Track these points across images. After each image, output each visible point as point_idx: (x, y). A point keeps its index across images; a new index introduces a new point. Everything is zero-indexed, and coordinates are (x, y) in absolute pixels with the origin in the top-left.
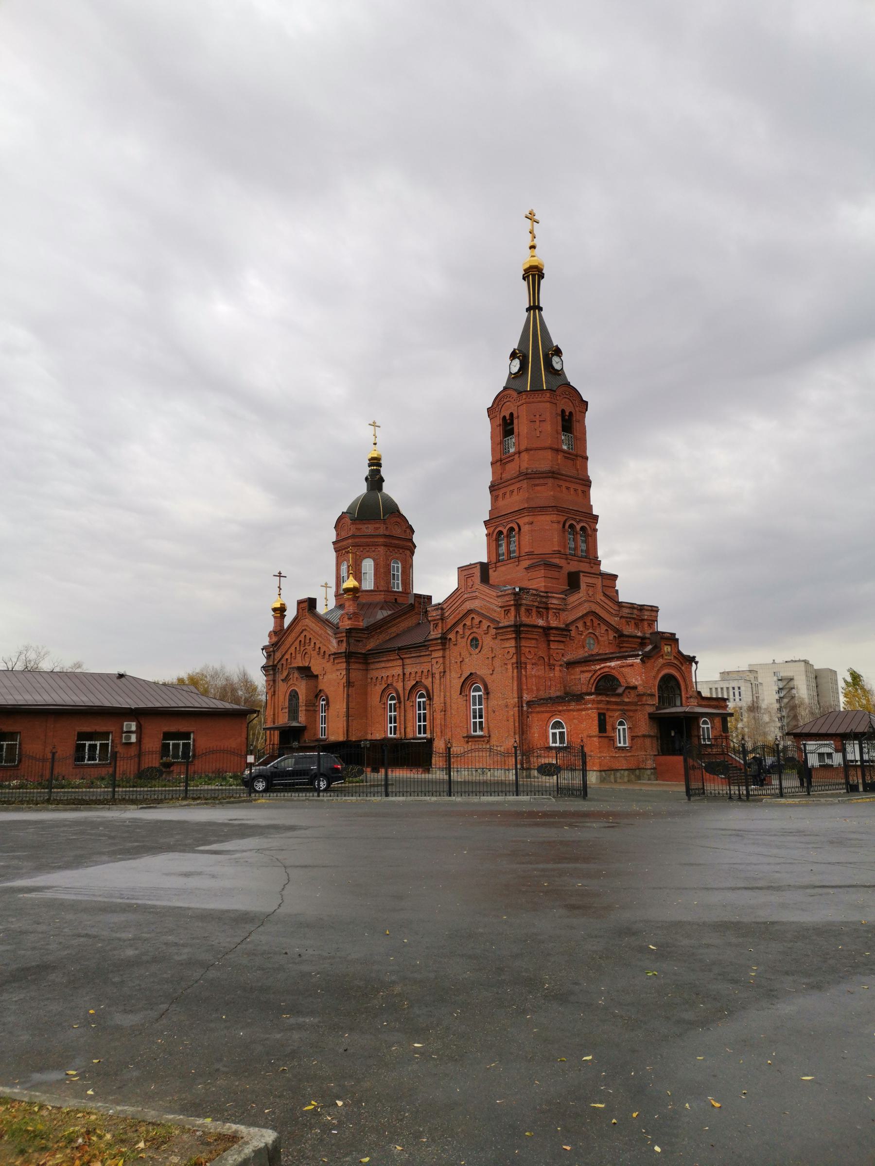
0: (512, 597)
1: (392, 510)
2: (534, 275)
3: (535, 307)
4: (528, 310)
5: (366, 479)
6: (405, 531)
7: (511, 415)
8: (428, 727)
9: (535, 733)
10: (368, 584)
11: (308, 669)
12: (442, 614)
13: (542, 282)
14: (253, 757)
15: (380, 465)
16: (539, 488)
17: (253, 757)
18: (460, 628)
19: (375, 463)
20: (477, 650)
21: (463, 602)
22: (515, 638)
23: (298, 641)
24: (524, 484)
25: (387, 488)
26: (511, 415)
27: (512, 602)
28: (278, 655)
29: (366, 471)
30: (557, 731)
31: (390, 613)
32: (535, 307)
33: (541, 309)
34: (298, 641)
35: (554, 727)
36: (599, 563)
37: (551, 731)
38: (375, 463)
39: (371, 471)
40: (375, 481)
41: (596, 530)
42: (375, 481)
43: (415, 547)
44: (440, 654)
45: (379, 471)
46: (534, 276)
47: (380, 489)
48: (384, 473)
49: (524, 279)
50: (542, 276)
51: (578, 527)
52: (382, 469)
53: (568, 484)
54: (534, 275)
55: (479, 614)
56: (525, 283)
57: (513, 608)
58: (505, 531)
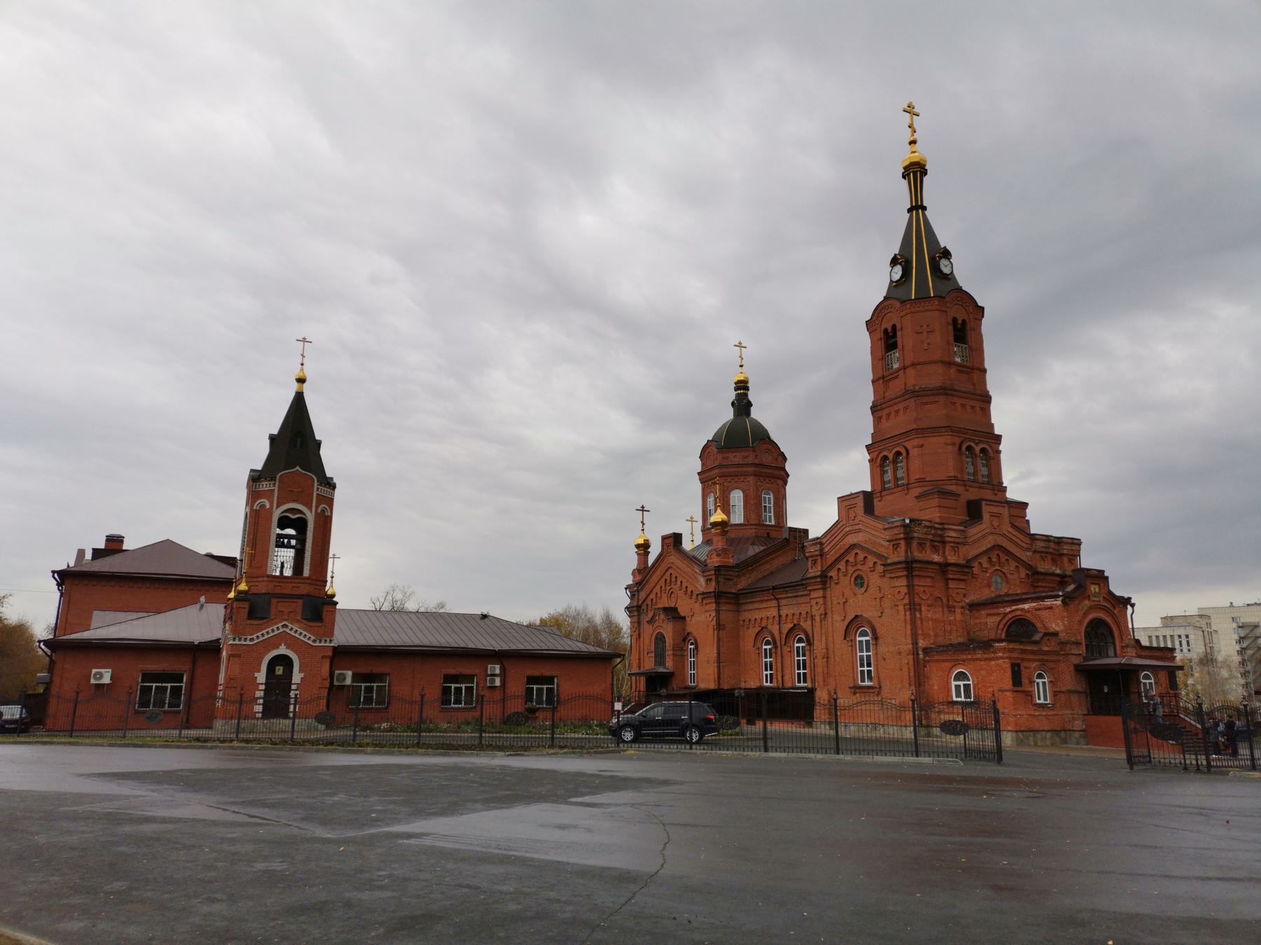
1: (762, 436)
2: (915, 172)
3: (917, 207)
4: (910, 211)
5: (733, 404)
7: (894, 327)
9: (934, 685)
10: (738, 518)
11: (675, 610)
12: (821, 550)
13: (925, 179)
15: (747, 389)
18: (842, 565)
19: (742, 386)
20: (863, 590)
22: (907, 577)
24: (911, 403)
25: (755, 413)
26: (894, 327)
28: (643, 595)
29: (732, 395)
30: (961, 683)
32: (917, 207)
33: (924, 208)
37: (954, 683)
38: (742, 386)
40: (742, 405)
41: (999, 452)
42: (742, 405)
45: (746, 395)
46: (915, 173)
47: (748, 414)
48: (751, 396)
49: (904, 177)
50: (924, 172)
51: (977, 449)
53: (896, 408)
54: (915, 172)
55: (863, 549)
56: (905, 182)
57: (902, 542)
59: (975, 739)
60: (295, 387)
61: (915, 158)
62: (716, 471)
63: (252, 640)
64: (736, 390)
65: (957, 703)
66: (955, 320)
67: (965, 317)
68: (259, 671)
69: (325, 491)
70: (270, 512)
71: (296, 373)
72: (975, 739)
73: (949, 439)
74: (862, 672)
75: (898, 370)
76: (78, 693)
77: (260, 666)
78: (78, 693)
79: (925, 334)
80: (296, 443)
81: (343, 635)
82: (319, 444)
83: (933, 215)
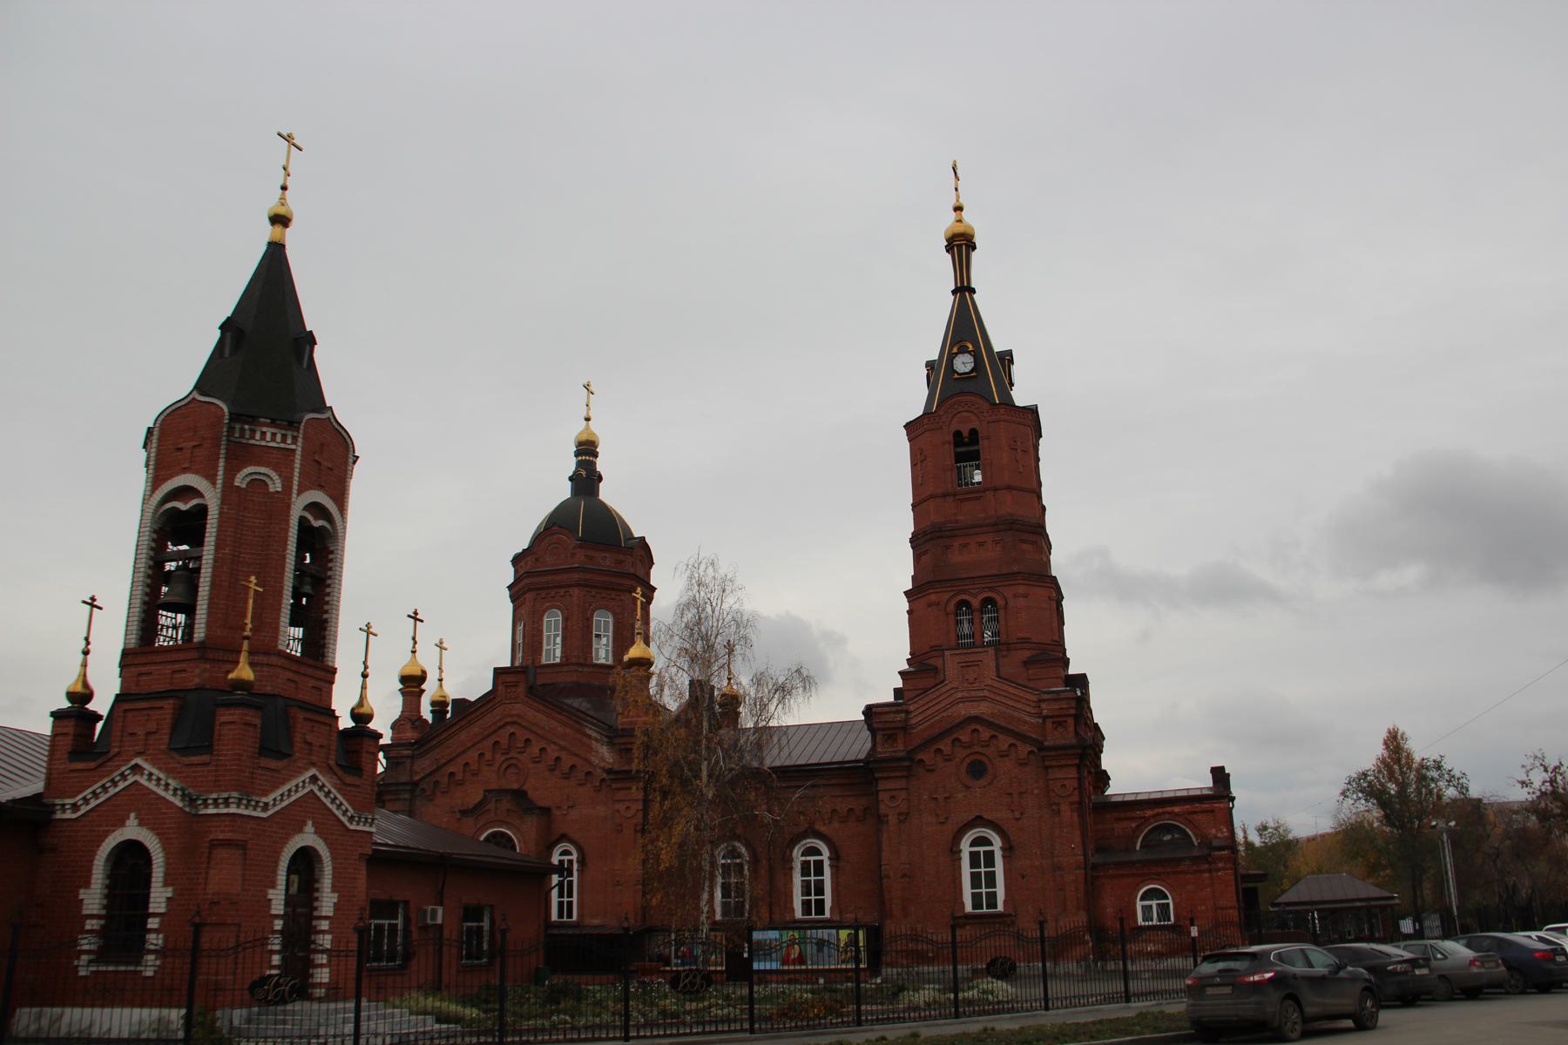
0: (1073, 704)
2: (961, 245)
3: (963, 290)
4: (954, 292)
9: (1109, 907)
11: (520, 795)
12: (906, 720)
14: (1402, 923)
16: (1025, 547)
17: (1402, 923)
18: (945, 745)
19: (587, 450)
20: (983, 782)
21: (952, 704)
22: (1078, 767)
23: (491, 741)
26: (973, 432)
27: (1073, 712)
28: (424, 765)
29: (570, 465)
30: (1154, 903)
31: (569, 701)
32: (963, 290)
33: (973, 291)
34: (491, 741)
35: (972, 845)
36: (1066, 662)
37: (1139, 905)
38: (587, 450)
39: (579, 464)
40: (586, 479)
42: (586, 479)
44: (902, 783)
46: (959, 246)
47: (594, 491)
48: (601, 465)
51: (976, 603)
54: (961, 245)
55: (990, 725)
56: (949, 257)
57: (1071, 721)
58: (976, 603)
60: (265, 233)
61: (960, 229)
62: (576, 576)
63: (75, 807)
64: (577, 454)
66: (958, 434)
67: (975, 425)
68: (87, 885)
70: (282, 503)
71: (271, 203)
74: (570, 895)
77: (275, 872)
80: (264, 356)
82: (913, 429)
83: (983, 300)
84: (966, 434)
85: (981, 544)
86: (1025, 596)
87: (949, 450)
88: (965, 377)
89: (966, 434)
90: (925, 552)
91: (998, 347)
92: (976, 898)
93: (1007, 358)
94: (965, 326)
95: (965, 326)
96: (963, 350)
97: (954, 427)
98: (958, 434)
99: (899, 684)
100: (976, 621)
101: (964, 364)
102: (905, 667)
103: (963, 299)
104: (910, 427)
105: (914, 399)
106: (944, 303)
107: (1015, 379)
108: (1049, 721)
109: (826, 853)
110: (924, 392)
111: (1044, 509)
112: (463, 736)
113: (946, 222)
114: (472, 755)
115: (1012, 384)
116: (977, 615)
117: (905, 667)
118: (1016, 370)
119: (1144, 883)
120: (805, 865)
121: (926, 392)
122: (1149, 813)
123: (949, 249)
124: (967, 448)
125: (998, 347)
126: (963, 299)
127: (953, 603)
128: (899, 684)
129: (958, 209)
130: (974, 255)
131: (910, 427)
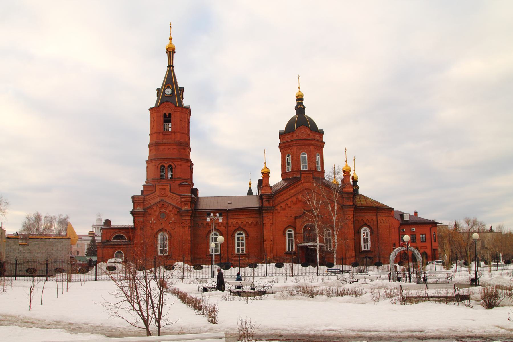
2: (171, 52)
3: (171, 66)
6: (309, 135)
7: (170, 114)
8: (293, 234)
15: (302, 100)
19: (300, 99)
22: (191, 216)
26: (170, 114)
29: (295, 104)
32: (171, 66)
35: (238, 235)
38: (300, 99)
40: (300, 109)
42: (300, 109)
43: (193, 165)
46: (170, 52)
51: (166, 166)
52: (304, 102)
53: (169, 147)
54: (171, 52)
56: (167, 54)
58: (166, 166)
59: (459, 255)
61: (171, 46)
64: (297, 100)
65: (160, 256)
66: (165, 114)
67: (170, 112)
69: (317, 137)
72: (459, 255)
73: (153, 164)
75: (171, 132)
76: (16, 261)
78: (16, 261)
79: (167, 119)
81: (358, 203)
84: (167, 114)
85: (169, 149)
86: (181, 165)
87: (162, 119)
88: (168, 96)
89: (167, 114)
90: (152, 150)
91: (180, 86)
92: (238, 250)
93: (182, 90)
94: (170, 79)
95: (170, 79)
96: (169, 87)
97: (164, 113)
98: (165, 114)
99: (142, 189)
100: (174, 171)
101: (169, 92)
102: (144, 183)
103: (170, 69)
104: (151, 109)
105: (153, 101)
106: (164, 70)
107: (184, 97)
108: (183, 204)
109: (244, 236)
110: (156, 99)
111: (189, 138)
112: (292, 191)
113: (166, 44)
114: (289, 202)
115: (183, 98)
116: (166, 170)
117: (144, 183)
118: (185, 94)
119: (116, 250)
120: (238, 238)
121: (156, 99)
122: (116, 231)
123: (167, 52)
124: (167, 119)
125: (180, 86)
126: (170, 69)
127: (160, 166)
128: (142, 189)
129: (171, 39)
130: (175, 55)
131: (151, 109)
